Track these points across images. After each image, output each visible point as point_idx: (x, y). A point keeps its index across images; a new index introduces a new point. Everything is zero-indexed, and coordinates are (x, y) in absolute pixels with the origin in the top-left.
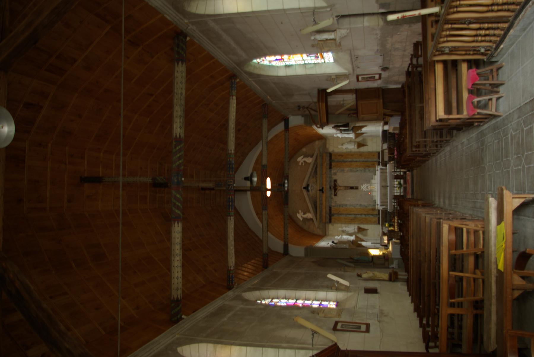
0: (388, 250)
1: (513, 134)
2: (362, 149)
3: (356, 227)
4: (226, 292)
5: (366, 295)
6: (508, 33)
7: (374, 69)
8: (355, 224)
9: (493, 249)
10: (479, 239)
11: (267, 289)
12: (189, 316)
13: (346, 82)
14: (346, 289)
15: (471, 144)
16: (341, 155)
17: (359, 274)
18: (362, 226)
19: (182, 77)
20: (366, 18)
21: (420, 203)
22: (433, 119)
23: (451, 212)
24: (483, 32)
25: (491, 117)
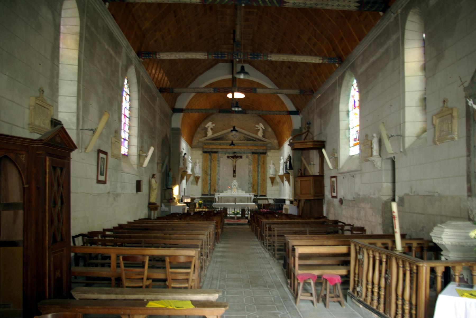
0: (178, 203)
1: (279, 315)
2: (269, 181)
3: (199, 175)
4: (134, 50)
5: (135, 182)
6: (374, 313)
7: (341, 192)
8: (202, 174)
9: (170, 296)
10: (181, 283)
11: (139, 90)
12: (108, 10)
14: (140, 164)
15: (270, 276)
16: (264, 163)
17: (155, 176)
18: (200, 181)
19: (344, 6)
20: (390, 185)
21: (219, 230)
22: (295, 243)
23: (209, 258)
24: (376, 290)
25: (295, 295)
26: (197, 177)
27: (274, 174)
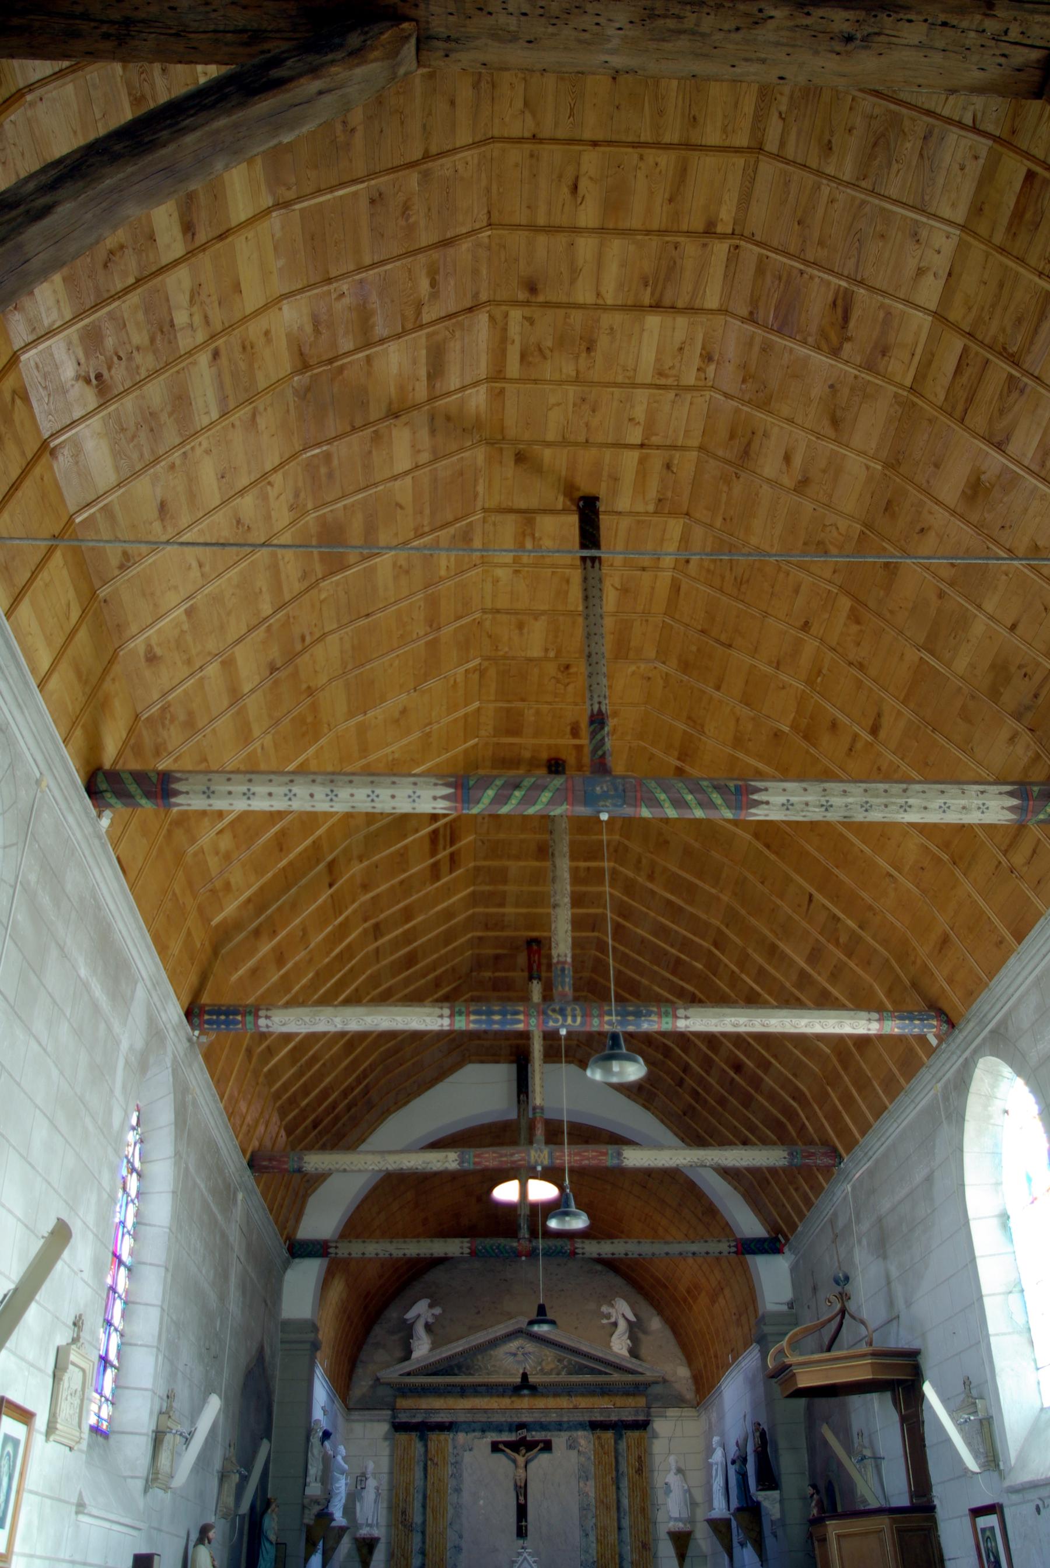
3: (376, 1533)
8: (389, 1526)
11: (177, 1154)
13: (971, 1463)
26: (364, 1539)
27: (685, 1515)
